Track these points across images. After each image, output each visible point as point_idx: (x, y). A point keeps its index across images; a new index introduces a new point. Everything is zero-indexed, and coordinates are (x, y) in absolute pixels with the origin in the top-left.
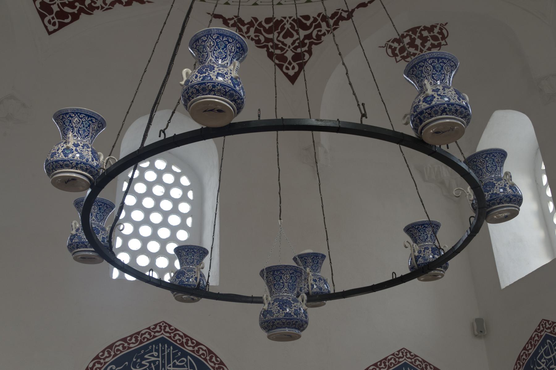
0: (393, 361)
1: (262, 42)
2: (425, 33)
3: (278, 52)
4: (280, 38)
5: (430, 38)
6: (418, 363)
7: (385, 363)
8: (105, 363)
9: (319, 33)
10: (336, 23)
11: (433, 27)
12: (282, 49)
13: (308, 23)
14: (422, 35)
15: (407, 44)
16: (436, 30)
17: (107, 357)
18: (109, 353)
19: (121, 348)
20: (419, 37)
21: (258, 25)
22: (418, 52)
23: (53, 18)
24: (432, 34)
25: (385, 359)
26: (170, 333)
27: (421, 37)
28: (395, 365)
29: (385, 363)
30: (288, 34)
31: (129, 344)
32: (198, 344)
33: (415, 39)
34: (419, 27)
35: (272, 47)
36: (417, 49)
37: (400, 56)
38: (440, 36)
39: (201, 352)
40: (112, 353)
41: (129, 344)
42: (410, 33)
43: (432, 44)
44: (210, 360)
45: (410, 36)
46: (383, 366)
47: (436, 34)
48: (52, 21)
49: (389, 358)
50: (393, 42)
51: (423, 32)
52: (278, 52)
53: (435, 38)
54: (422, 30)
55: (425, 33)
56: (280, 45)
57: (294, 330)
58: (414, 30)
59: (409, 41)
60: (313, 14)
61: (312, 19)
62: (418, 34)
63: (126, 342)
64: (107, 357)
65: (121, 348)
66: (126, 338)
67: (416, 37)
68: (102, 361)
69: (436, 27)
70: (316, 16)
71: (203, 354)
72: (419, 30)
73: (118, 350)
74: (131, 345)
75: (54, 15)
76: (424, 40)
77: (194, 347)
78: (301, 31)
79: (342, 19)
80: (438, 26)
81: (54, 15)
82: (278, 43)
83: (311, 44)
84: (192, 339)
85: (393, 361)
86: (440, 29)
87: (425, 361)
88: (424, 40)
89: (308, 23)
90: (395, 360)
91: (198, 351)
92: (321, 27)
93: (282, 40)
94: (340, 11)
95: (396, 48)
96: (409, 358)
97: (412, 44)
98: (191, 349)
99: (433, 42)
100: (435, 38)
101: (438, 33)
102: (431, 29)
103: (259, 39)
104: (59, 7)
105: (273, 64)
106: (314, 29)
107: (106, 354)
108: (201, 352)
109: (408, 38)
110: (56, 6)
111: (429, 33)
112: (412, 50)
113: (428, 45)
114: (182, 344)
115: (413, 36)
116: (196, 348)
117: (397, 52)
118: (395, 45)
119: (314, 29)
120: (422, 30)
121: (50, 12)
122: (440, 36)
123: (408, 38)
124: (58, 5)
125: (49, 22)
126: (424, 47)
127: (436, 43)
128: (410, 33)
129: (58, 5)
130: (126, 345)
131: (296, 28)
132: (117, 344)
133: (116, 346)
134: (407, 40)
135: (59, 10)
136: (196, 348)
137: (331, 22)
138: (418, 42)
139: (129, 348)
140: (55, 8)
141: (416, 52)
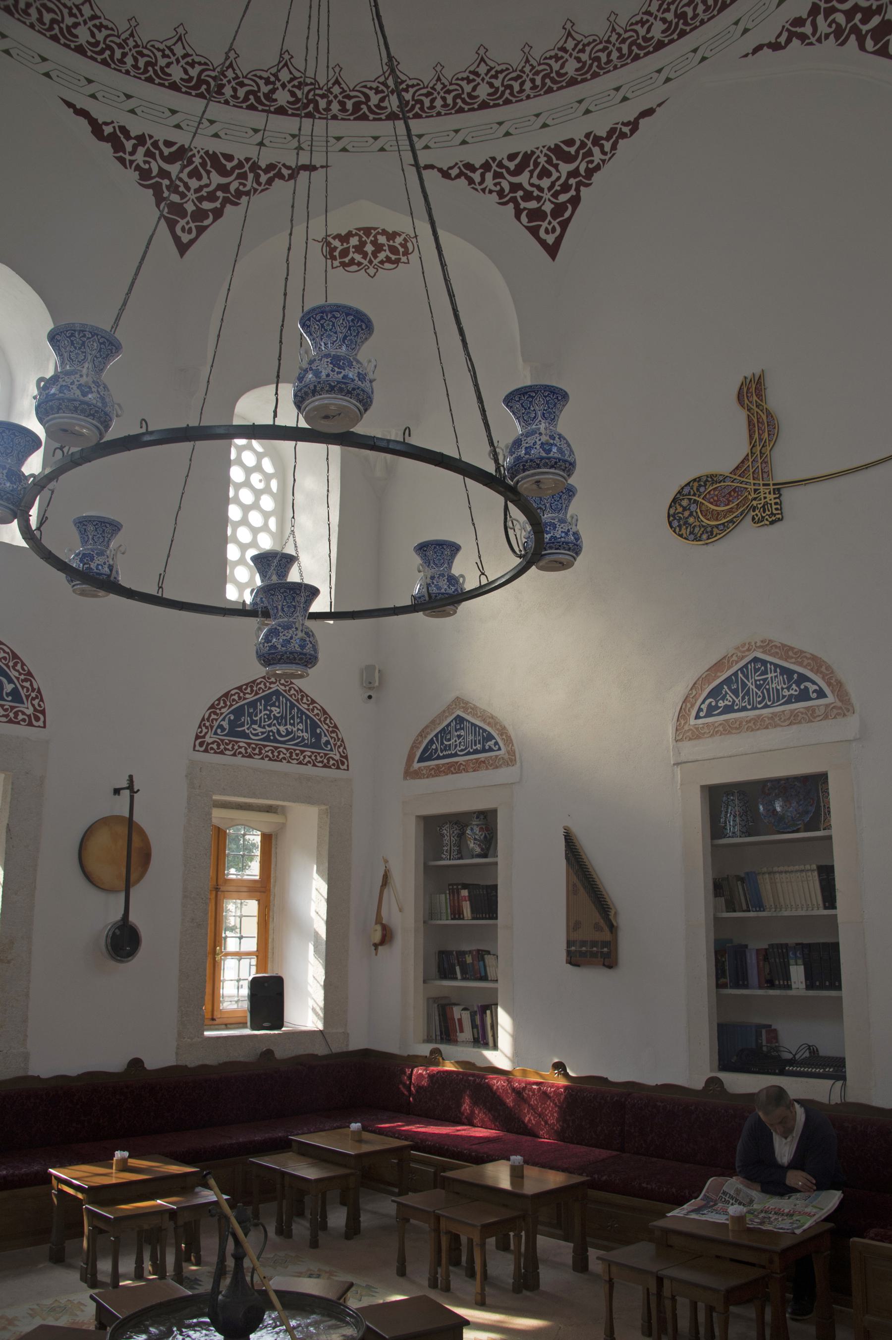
0: (262, 686)
1: (154, 174)
2: (382, 239)
3: (175, 198)
4: (184, 176)
5: (386, 248)
6: (292, 692)
7: (252, 687)
8: (222, 714)
9: (241, 188)
10: (270, 182)
11: (395, 235)
12: (183, 196)
13: (229, 166)
14: (376, 239)
15: (353, 247)
16: (399, 240)
17: (222, 707)
18: (225, 703)
19: (236, 697)
20: (372, 242)
21: (152, 144)
22: (366, 262)
23: (188, 223)
24: (391, 243)
25: (254, 682)
26: (285, 686)
27: (374, 243)
28: (264, 691)
29: (252, 687)
30: (195, 174)
31: (245, 694)
32: (313, 702)
33: (365, 243)
34: (375, 229)
35: (168, 187)
36: (365, 257)
37: (339, 260)
38: (401, 250)
39: (316, 711)
40: (228, 703)
41: (245, 694)
42: (361, 233)
43: (387, 257)
44: (324, 721)
45: (360, 237)
46: (249, 690)
47: (396, 245)
48: (187, 227)
49: (258, 681)
50: (334, 238)
51: (379, 237)
52: (175, 198)
53: (393, 250)
54: (378, 233)
55: (382, 239)
56: (182, 189)
57: (294, 666)
58: (367, 231)
59: (358, 243)
60: (240, 154)
61: (235, 162)
62: (371, 238)
63: (242, 691)
64: (222, 707)
65: (236, 697)
66: (242, 686)
67: (368, 241)
68: (218, 711)
69: (400, 235)
70: (242, 159)
71: (318, 714)
72: (374, 233)
73: (234, 700)
74: (247, 696)
75: (188, 218)
76: (378, 248)
77: (308, 705)
78: (214, 175)
79: (280, 176)
80: (404, 236)
81: (188, 218)
82: (178, 182)
83: (226, 201)
84: (307, 696)
85: (262, 686)
86: (405, 240)
87: (301, 691)
88: (378, 248)
89: (229, 166)
90: (265, 684)
91: (313, 710)
92: (246, 179)
93: (186, 179)
94: (280, 165)
95: (336, 248)
96: (283, 685)
97: (360, 249)
98: (306, 706)
99: (390, 255)
100: (393, 250)
101: (401, 244)
102: (392, 236)
103: (150, 168)
104: (195, 204)
105: (158, 213)
106: (236, 179)
107: (222, 704)
108: (316, 711)
109: (357, 238)
110: (190, 202)
111: (388, 240)
112: (358, 257)
113: (382, 256)
114: (297, 701)
115: (364, 238)
116: (311, 707)
117: (336, 254)
118: (336, 243)
119: (236, 179)
120: (378, 233)
121: (183, 213)
122: (401, 250)
123: (357, 238)
124: (193, 201)
125: (183, 229)
126: (376, 257)
127: (393, 257)
128: (361, 233)
129: (193, 201)
130: (242, 695)
131: (208, 168)
132: (233, 692)
133: (232, 695)
134: (354, 241)
135: (194, 208)
136: (311, 707)
137: (264, 178)
138: (369, 248)
139: (245, 699)
140: (190, 207)
141: (362, 261)
